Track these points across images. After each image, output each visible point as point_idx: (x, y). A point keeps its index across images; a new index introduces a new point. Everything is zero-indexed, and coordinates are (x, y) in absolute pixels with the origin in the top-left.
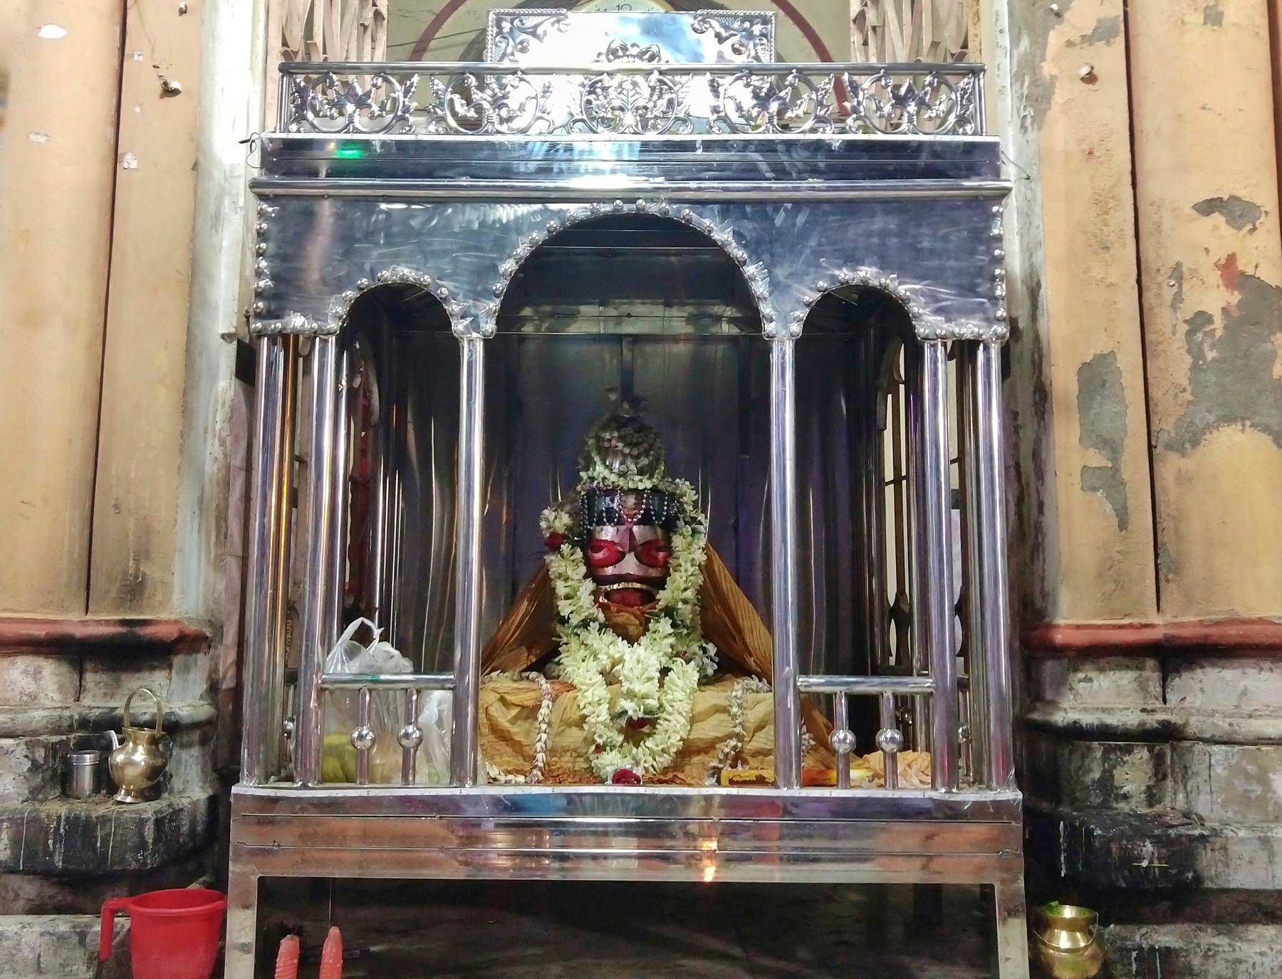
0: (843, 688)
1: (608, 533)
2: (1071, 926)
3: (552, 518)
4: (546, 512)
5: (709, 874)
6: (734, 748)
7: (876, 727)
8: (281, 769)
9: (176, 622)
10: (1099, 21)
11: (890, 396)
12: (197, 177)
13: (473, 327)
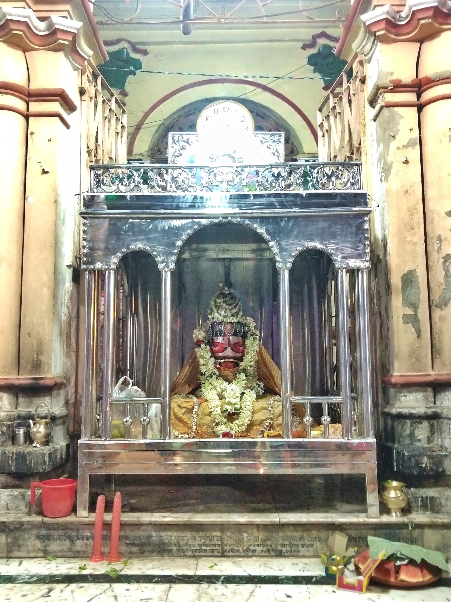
0: (308, 401)
1: (220, 339)
2: (395, 488)
3: (197, 334)
4: (195, 331)
5: (262, 471)
6: (270, 423)
7: (321, 415)
8: (96, 434)
9: (53, 378)
10: (410, 139)
11: (333, 282)
12: (56, 206)
13: (166, 268)
